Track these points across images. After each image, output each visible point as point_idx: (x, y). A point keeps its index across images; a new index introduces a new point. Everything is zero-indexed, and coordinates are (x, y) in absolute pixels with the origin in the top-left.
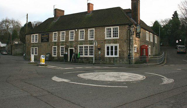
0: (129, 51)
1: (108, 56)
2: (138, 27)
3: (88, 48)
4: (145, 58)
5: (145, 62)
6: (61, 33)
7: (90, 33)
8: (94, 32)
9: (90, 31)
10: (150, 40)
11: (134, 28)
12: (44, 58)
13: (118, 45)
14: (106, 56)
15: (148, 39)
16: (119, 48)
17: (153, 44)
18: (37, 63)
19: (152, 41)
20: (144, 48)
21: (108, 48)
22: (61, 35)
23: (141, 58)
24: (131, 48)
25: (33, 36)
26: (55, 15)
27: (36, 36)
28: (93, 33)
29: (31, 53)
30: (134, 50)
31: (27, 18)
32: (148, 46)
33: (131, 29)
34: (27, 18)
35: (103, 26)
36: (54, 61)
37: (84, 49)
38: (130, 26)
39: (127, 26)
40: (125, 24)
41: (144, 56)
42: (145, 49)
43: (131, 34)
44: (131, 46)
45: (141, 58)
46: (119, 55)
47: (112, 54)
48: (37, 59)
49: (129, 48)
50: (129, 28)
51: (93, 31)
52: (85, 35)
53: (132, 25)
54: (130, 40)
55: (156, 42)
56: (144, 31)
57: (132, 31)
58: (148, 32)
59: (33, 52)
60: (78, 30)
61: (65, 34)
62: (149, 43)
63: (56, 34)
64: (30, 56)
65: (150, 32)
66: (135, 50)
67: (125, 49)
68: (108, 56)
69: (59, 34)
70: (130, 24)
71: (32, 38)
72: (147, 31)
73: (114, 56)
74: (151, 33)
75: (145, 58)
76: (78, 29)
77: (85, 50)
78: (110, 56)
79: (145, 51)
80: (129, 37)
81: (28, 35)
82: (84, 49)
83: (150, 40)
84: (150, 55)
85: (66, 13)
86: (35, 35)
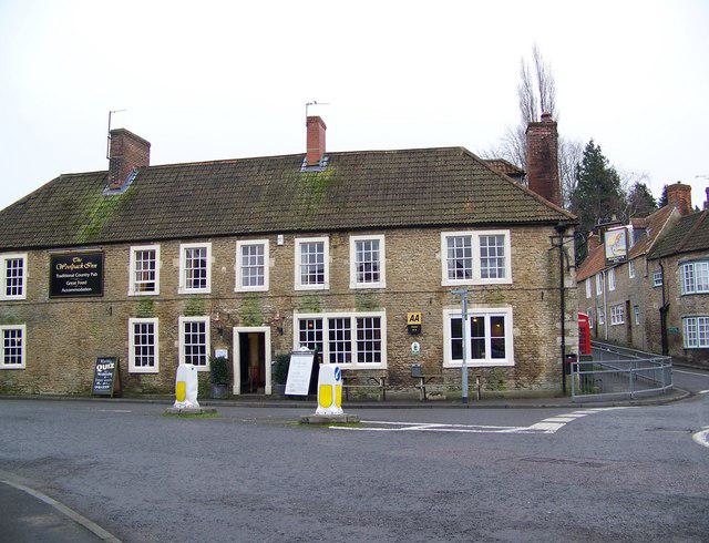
0: (559, 339)
21: (457, 326)
37: (326, 330)
38: (561, 230)
44: (567, 316)
49: (559, 325)
52: (333, 267)
67: (543, 326)
69: (169, 258)
70: (560, 224)
73: (488, 361)
76: (291, 233)
80: (557, 276)
82: (326, 330)
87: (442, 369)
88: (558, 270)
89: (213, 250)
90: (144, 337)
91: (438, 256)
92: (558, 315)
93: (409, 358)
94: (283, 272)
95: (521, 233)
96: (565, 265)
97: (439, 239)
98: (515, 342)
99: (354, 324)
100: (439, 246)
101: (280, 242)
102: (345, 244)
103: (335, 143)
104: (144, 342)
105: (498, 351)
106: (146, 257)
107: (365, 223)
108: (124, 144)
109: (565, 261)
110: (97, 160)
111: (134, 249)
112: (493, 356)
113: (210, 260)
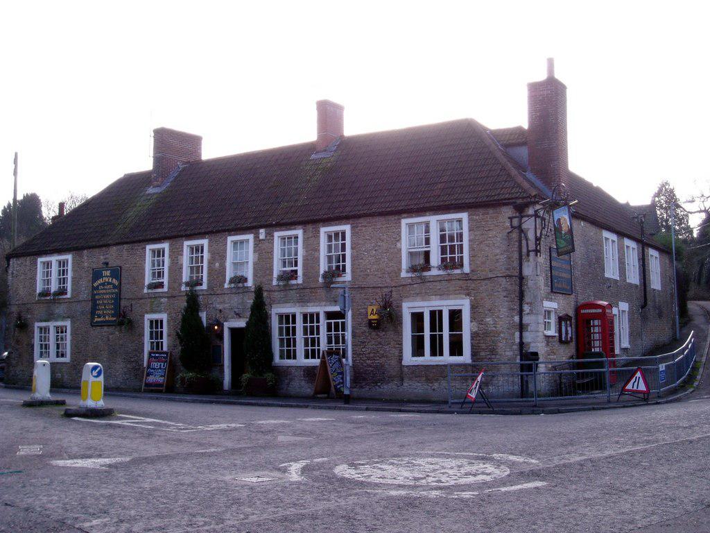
0: (517, 334)
1: (419, 360)
2: (563, 215)
3: (294, 322)
4: (601, 365)
5: (597, 384)
6: (186, 251)
7: (330, 247)
8: (348, 242)
9: (330, 238)
10: (622, 271)
11: (538, 221)
12: (101, 378)
13: (464, 305)
14: (409, 359)
15: (611, 272)
16: (473, 319)
17: (642, 297)
18: (68, 401)
19: (634, 278)
20: (595, 316)
21: (417, 318)
22: (185, 260)
23: (579, 366)
24: (526, 319)
25: (48, 265)
26: (158, 160)
27: (62, 264)
28: (344, 246)
29: (37, 350)
30: (541, 327)
31: (15, 173)
32: (610, 306)
33: (529, 224)
34: (15, 173)
35: (140, 241)
36: (398, 403)
37: (323, 323)
38: (520, 209)
39: (508, 212)
40: (494, 204)
41: (599, 355)
42: (596, 322)
43: (529, 251)
44: (526, 308)
45: (579, 366)
46: (474, 354)
47: (436, 350)
48: (66, 382)
49: (517, 319)
50: (515, 222)
51: (344, 239)
52: (305, 260)
53: (527, 205)
54: (521, 278)
55: (656, 283)
56: (592, 231)
57: (531, 235)
58: (613, 237)
59: (47, 347)
60: (270, 236)
61: (206, 255)
62: (618, 289)
63: (159, 253)
64: (31, 364)
65: (621, 234)
66: (547, 326)
67: (501, 319)
68: (419, 360)
69: (176, 254)
70: (519, 201)
71: (70, 275)
72: (606, 234)
73: (447, 358)
74: (627, 242)
75: (601, 365)
76: (272, 226)
77: (305, 333)
78: (427, 359)
79: (597, 330)
80: (516, 264)
81: (21, 260)
82: (323, 323)
83: (622, 271)
84: (625, 350)
85: (209, 152)
86: (54, 259)
87: (402, 367)
88: (516, 255)
89: (210, 246)
90: (312, 327)
91: (398, 245)
92: (517, 307)
93: (372, 355)
94: (112, 280)
95: (480, 214)
96: (524, 250)
97: (400, 227)
98: (472, 338)
99: (299, 319)
100: (399, 234)
101: (262, 236)
102: (316, 235)
103: (353, 127)
104: (312, 333)
105: (456, 349)
106: (197, 250)
107: (337, 213)
108: (329, 114)
109: (524, 242)
110: (142, 161)
111: (149, 247)
112: (452, 353)
113: (206, 255)
